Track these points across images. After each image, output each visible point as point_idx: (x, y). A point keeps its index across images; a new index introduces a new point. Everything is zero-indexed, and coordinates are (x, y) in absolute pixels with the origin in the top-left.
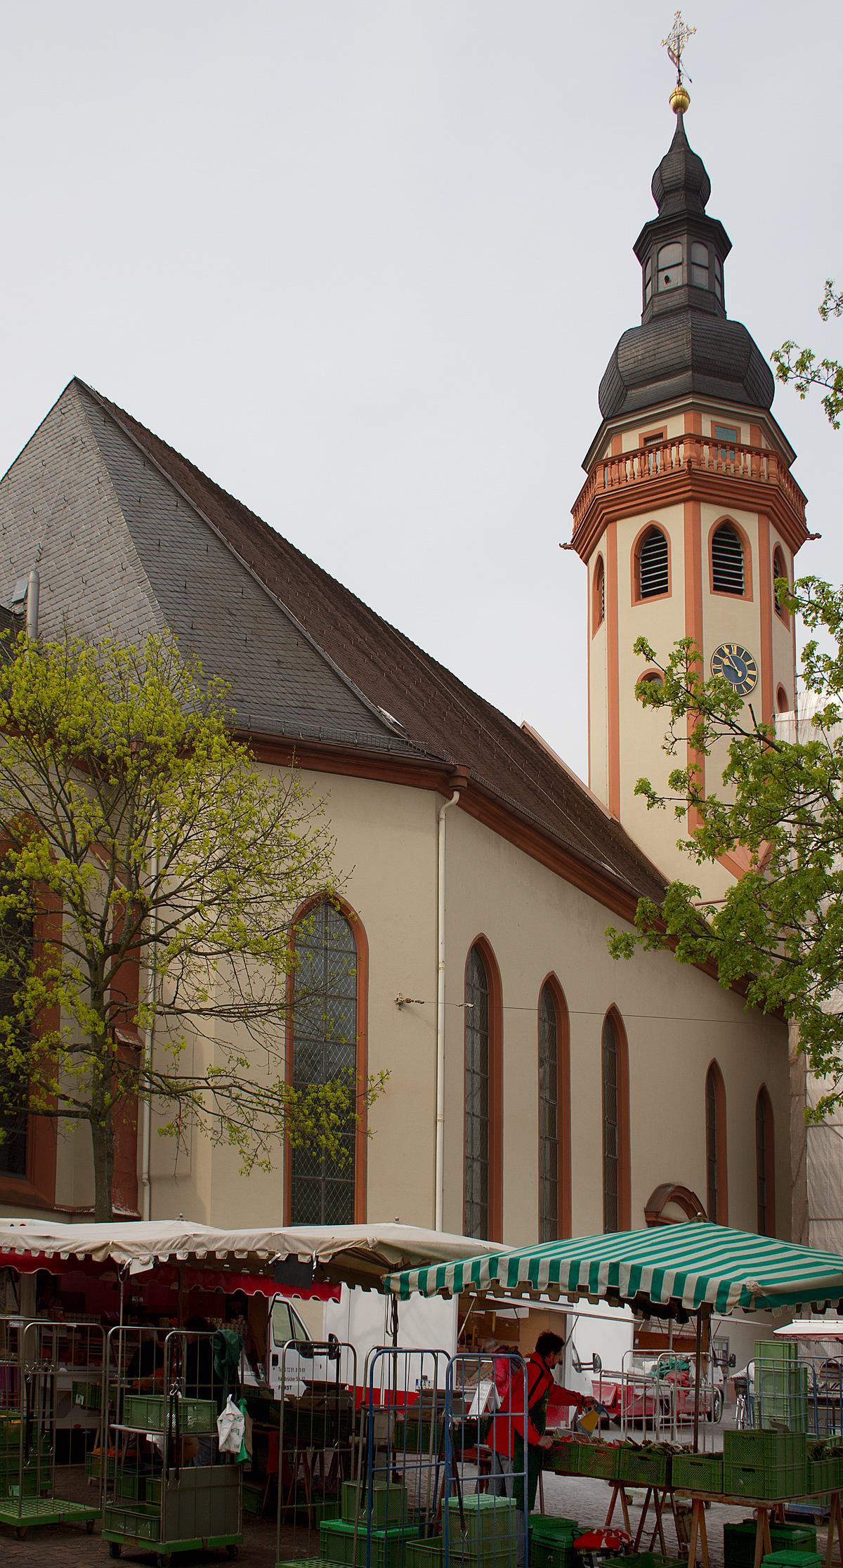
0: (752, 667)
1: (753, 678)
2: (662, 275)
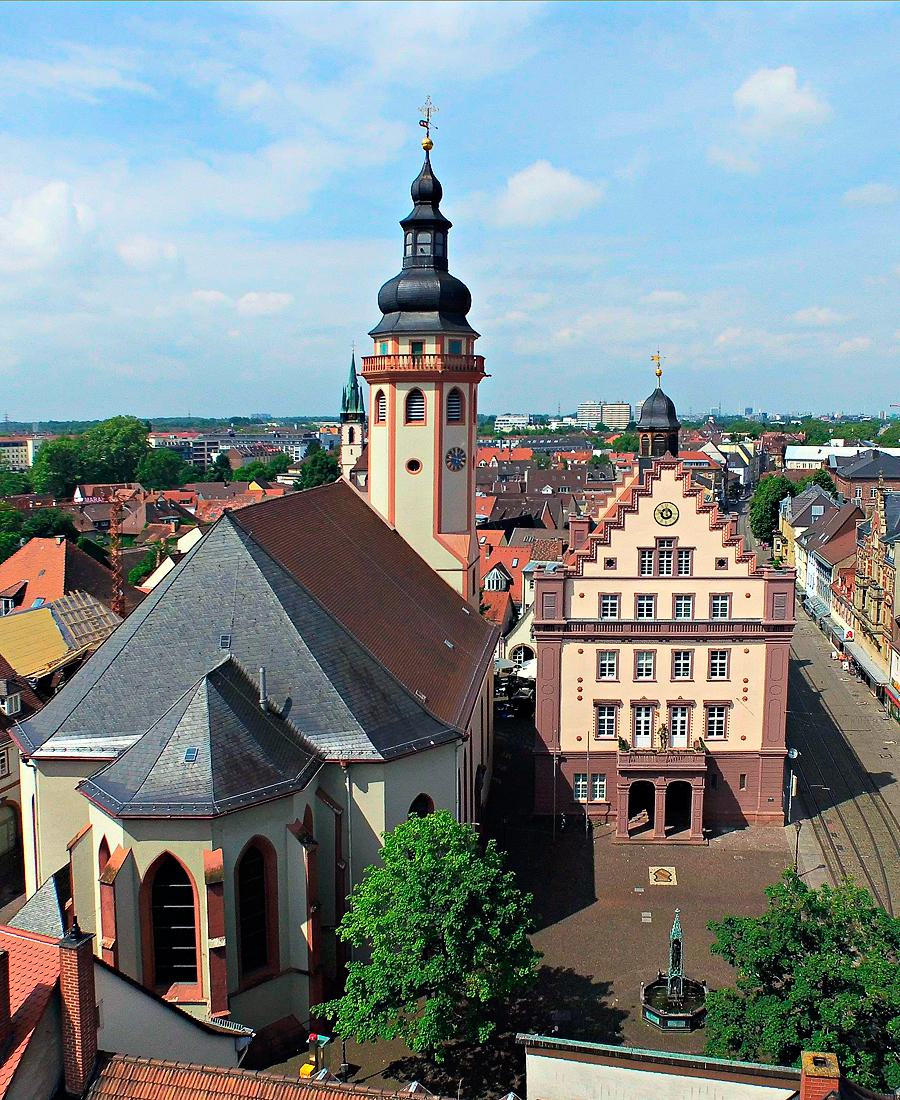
0: (464, 456)
1: (464, 461)
2: (419, 247)
